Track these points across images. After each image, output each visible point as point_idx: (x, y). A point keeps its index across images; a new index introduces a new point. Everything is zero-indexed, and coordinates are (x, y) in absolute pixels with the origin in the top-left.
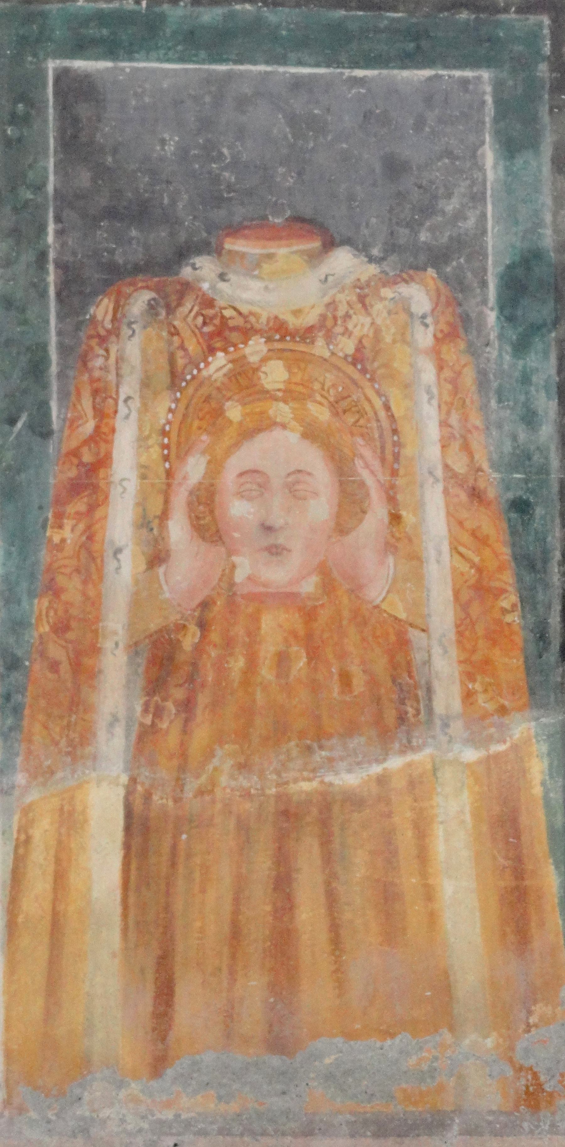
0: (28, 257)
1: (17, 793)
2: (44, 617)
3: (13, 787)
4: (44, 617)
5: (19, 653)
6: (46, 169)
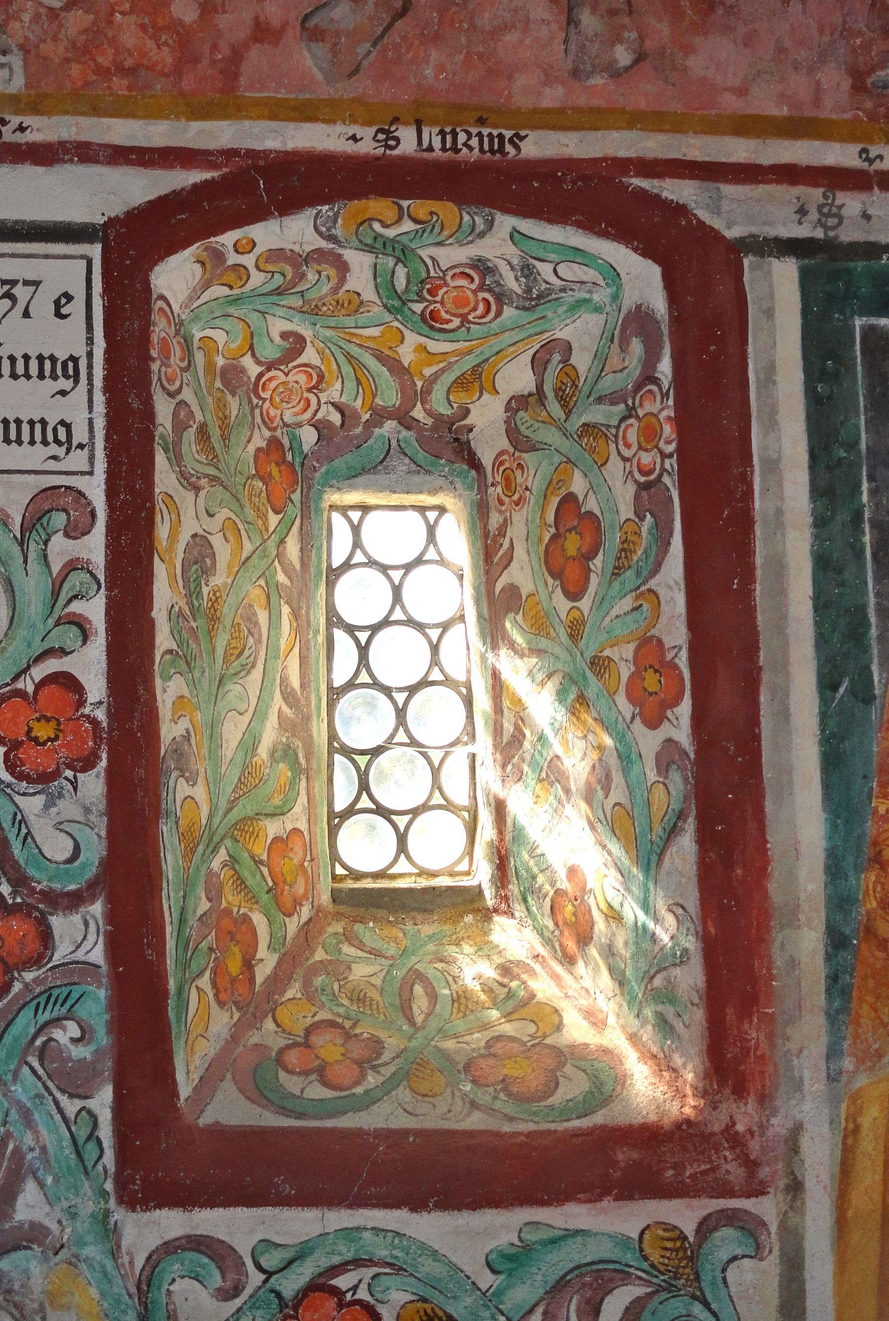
0: (843, 516)
1: (844, 1078)
2: (871, 892)
3: (840, 1073)
4: (871, 892)
5: (847, 931)
6: (857, 427)
